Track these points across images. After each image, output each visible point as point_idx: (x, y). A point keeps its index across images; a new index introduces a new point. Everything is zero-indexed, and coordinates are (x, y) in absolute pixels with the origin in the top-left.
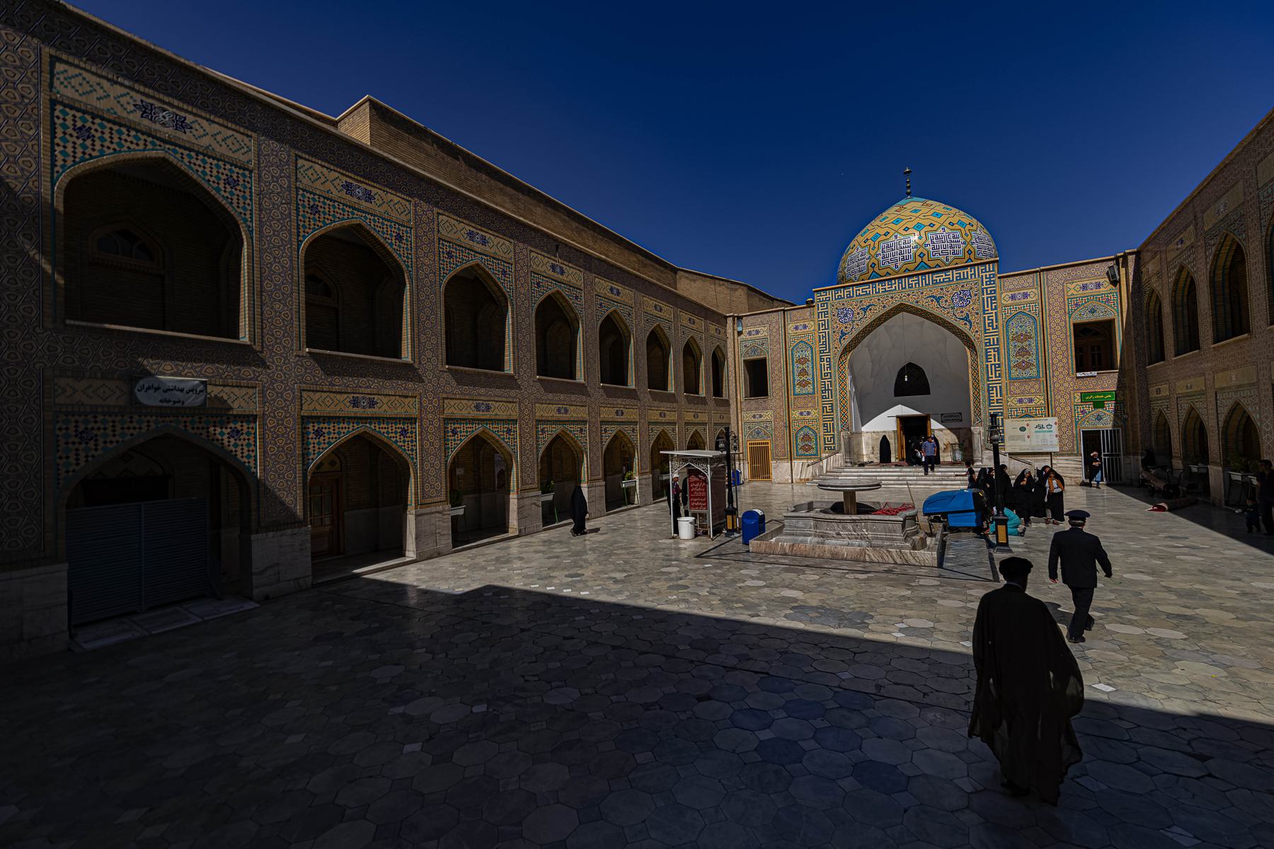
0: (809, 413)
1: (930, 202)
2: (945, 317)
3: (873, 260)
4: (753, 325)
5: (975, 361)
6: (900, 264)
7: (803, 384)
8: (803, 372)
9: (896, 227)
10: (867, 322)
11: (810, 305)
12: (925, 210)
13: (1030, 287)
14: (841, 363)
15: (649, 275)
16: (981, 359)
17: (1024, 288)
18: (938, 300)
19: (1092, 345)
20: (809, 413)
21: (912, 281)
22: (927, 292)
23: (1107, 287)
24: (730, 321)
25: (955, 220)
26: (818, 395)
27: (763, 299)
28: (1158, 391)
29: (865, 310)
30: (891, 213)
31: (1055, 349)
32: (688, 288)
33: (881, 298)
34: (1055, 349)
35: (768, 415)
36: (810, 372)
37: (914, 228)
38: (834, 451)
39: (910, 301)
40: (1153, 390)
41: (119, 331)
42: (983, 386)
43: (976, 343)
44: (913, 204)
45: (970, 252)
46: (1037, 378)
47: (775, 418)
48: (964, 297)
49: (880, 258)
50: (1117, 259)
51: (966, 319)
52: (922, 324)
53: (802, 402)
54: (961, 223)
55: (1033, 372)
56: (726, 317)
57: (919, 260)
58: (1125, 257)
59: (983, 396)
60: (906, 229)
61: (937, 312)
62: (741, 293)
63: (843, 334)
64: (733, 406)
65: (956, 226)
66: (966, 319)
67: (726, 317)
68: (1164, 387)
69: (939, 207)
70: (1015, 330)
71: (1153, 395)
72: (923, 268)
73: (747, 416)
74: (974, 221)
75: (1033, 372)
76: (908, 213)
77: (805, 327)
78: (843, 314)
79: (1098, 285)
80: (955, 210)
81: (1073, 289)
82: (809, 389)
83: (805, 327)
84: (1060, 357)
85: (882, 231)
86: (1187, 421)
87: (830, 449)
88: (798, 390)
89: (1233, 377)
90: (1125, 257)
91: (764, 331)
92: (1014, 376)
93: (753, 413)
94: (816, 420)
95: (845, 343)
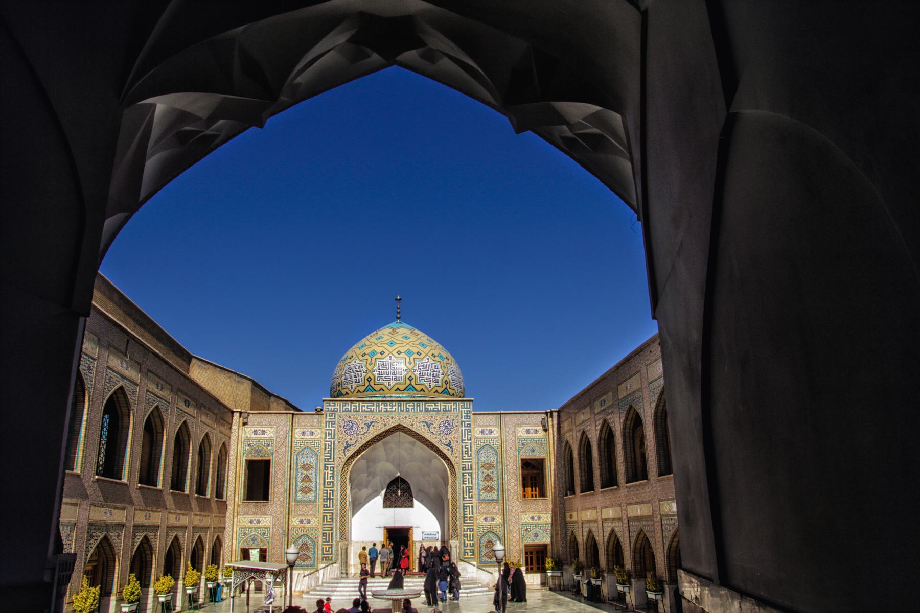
0: (309, 521)
1: (416, 331)
2: (433, 441)
3: (370, 375)
4: (259, 424)
5: (454, 482)
6: (393, 383)
7: (306, 491)
8: (307, 479)
9: (391, 349)
10: (370, 437)
11: (319, 412)
12: (413, 338)
13: (495, 426)
14: (343, 473)
15: (172, 360)
16: (459, 481)
17: (490, 426)
18: (429, 425)
19: (532, 473)
20: (309, 521)
21: (409, 406)
22: (420, 418)
23: (541, 433)
24: (236, 415)
25: (436, 352)
26: (320, 503)
27: (263, 398)
28: (571, 516)
29: (368, 425)
30: (385, 332)
31: (509, 478)
32: (199, 374)
33: (383, 417)
34: (509, 478)
35: (266, 521)
36: (313, 479)
37: (399, 353)
38: (329, 561)
39: (406, 423)
40: (568, 515)
41: (69, 385)
42: (460, 503)
43: (456, 466)
44: (404, 330)
45: (446, 382)
46: (497, 501)
47: (274, 525)
48: (448, 426)
49: (376, 373)
50: (546, 413)
51: (449, 445)
52: (413, 444)
53: (302, 509)
54: (441, 357)
55: (494, 495)
56: (233, 412)
57: (408, 382)
58: (551, 413)
59: (460, 515)
60: (399, 353)
61: (427, 436)
62: (246, 387)
63: (348, 446)
64: (230, 509)
65: (437, 358)
66: (449, 445)
67: (233, 412)
68: (574, 514)
69: (424, 338)
70: (483, 459)
71: (568, 519)
72: (411, 390)
73: (244, 520)
74: (449, 356)
75: (494, 495)
76: (399, 338)
77: (312, 433)
78: (349, 427)
79: (536, 431)
80: (435, 343)
81: (521, 432)
82: (311, 496)
83: (312, 433)
84: (512, 484)
85: (379, 350)
86: (587, 540)
87: (327, 559)
88: (300, 496)
89: (610, 513)
90: (551, 413)
91: (270, 433)
92: (482, 497)
93: (251, 517)
94: (316, 529)
95: (349, 454)
